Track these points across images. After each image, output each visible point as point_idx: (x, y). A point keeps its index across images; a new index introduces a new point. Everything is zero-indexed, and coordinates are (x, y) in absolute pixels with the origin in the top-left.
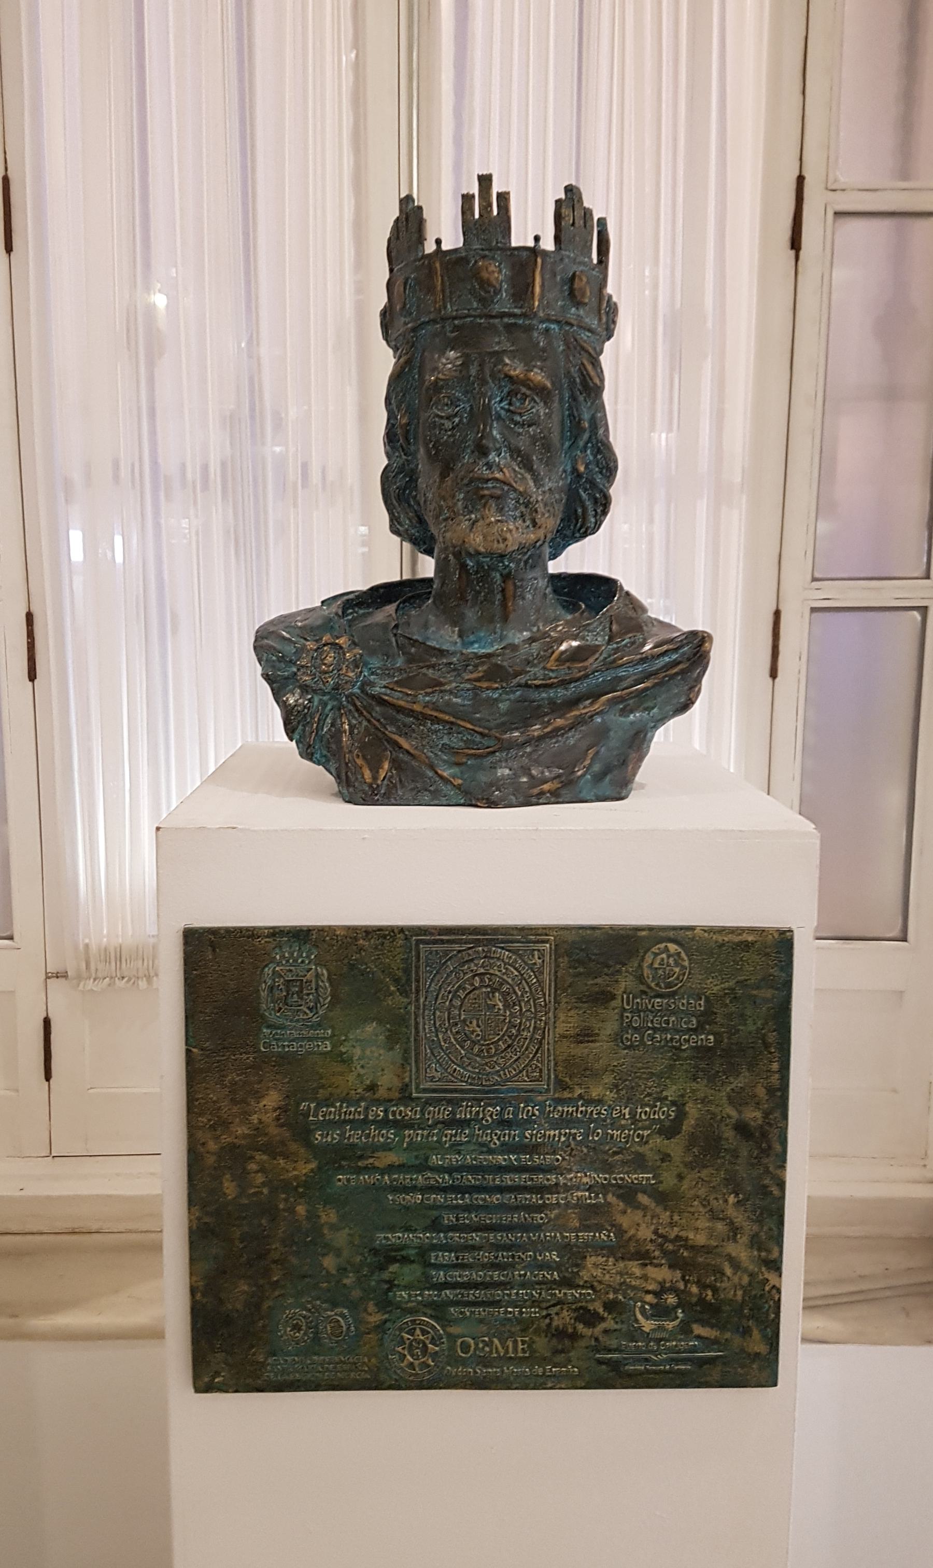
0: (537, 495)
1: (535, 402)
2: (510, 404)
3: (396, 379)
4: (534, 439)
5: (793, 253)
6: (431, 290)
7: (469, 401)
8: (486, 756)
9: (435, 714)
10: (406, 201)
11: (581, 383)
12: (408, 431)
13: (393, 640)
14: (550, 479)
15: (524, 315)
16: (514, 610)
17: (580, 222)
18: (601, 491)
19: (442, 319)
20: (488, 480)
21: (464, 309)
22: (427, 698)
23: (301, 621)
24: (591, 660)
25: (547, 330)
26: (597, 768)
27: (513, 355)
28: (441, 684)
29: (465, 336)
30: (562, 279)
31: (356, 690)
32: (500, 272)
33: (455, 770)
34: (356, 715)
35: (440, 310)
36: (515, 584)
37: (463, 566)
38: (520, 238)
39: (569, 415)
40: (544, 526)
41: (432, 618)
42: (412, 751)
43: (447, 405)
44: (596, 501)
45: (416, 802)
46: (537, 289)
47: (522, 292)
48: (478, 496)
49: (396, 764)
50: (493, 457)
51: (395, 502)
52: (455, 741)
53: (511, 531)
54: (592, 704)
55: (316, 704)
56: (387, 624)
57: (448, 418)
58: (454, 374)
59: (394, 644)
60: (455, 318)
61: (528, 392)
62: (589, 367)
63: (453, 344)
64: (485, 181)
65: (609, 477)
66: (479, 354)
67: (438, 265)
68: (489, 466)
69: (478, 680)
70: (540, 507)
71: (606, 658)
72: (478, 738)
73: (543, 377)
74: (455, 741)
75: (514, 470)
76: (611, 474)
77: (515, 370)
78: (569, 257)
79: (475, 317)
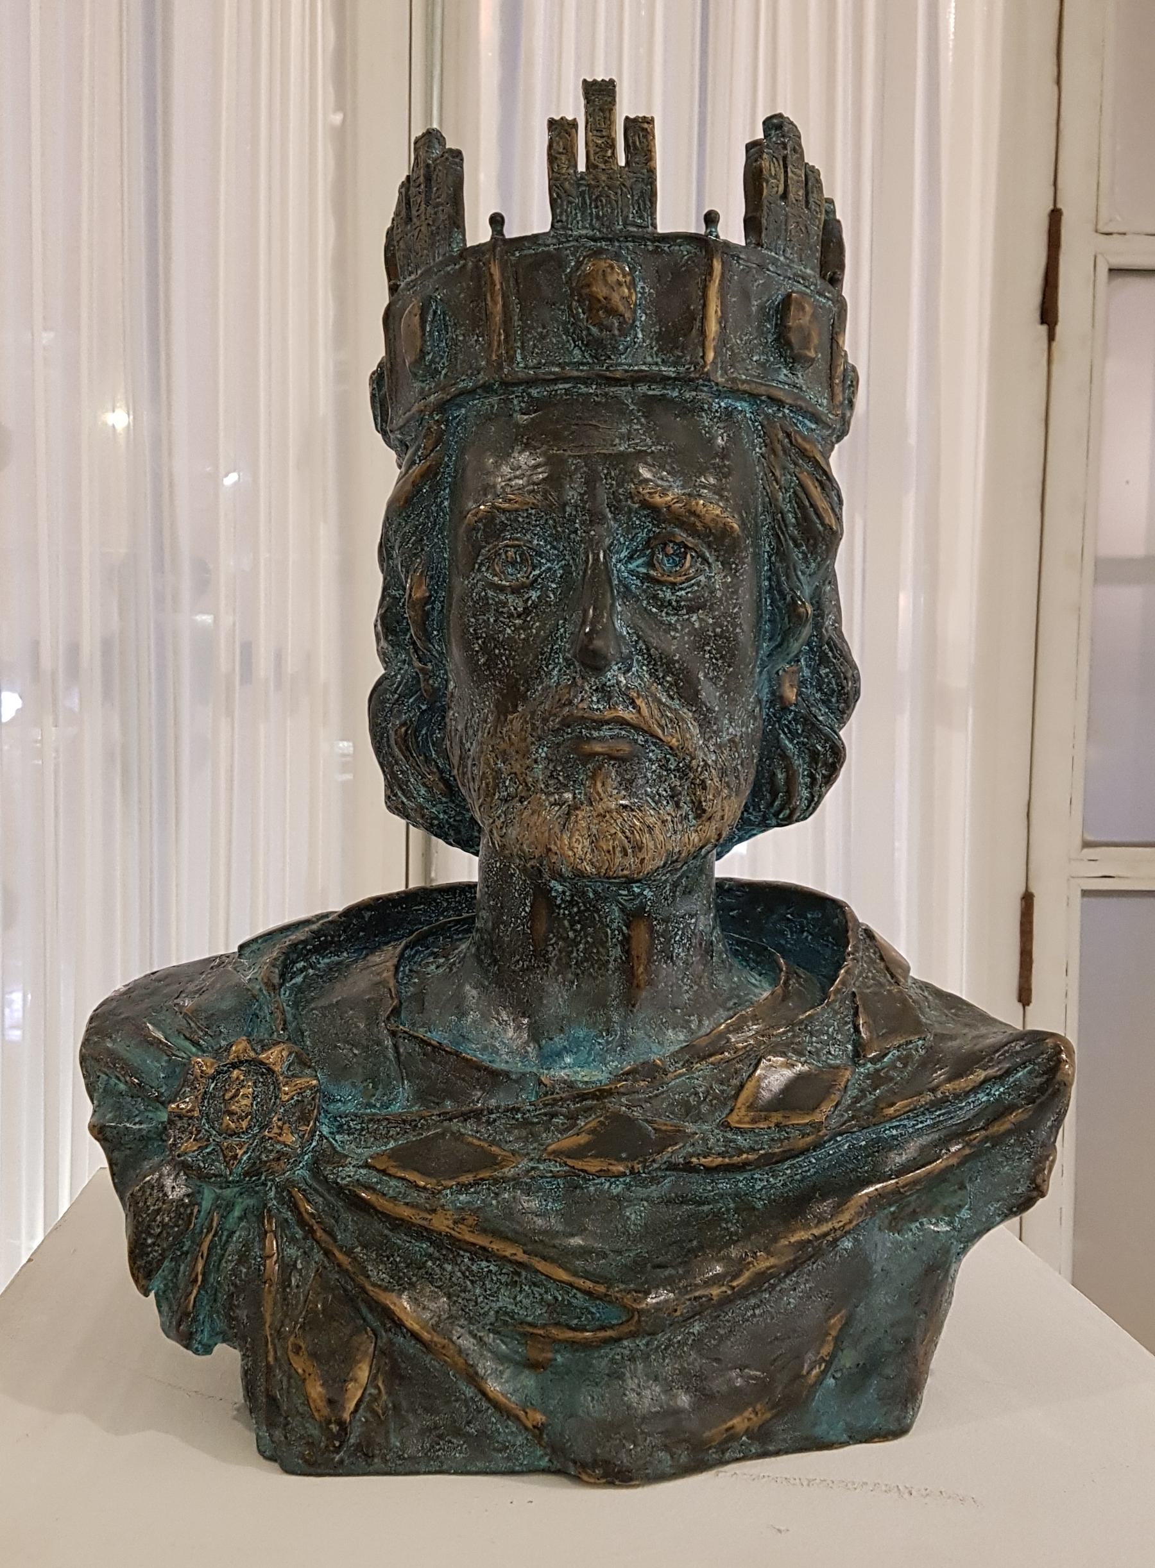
0: (704, 753)
1: (705, 560)
2: (650, 564)
3: (403, 508)
4: (701, 639)
5: (1043, 329)
6: (479, 321)
7: (560, 557)
8: (598, 1347)
9: (482, 1241)
10: (431, 138)
11: (798, 525)
12: (427, 615)
13: (388, 1042)
14: (731, 720)
15: (685, 381)
16: (650, 983)
17: (797, 193)
18: (828, 739)
19: (505, 384)
20: (600, 724)
21: (553, 364)
22: (462, 1197)
23: (191, 996)
24: (827, 1108)
25: (729, 413)
26: (848, 1359)
27: (658, 462)
28: (493, 1162)
29: (553, 420)
30: (762, 308)
31: (301, 1172)
32: (632, 285)
33: (529, 1380)
34: (299, 1234)
35: (501, 367)
36: (651, 929)
37: (542, 893)
38: (674, 215)
39: (770, 589)
40: (718, 816)
41: (470, 992)
42: (426, 1336)
43: (513, 563)
44: (814, 756)
45: (435, 1465)
46: (713, 327)
47: (679, 329)
48: (578, 755)
49: (392, 1369)
50: (614, 675)
51: (397, 752)
52: (525, 1304)
53: (650, 829)
54: (837, 1209)
55: (206, 1204)
56: (380, 1001)
57: (516, 591)
58: (530, 499)
59: (391, 1053)
60: (531, 383)
61: (691, 541)
62: (816, 492)
63: (526, 438)
64: (599, 95)
65: (843, 712)
66: (586, 458)
67: (496, 271)
68: (605, 692)
69: (578, 1153)
70: (713, 780)
71: (856, 1100)
72: (580, 1300)
73: (724, 510)
74: (525, 1304)
75: (659, 701)
76: (848, 707)
77: (664, 493)
78: (774, 262)
79: (577, 380)
